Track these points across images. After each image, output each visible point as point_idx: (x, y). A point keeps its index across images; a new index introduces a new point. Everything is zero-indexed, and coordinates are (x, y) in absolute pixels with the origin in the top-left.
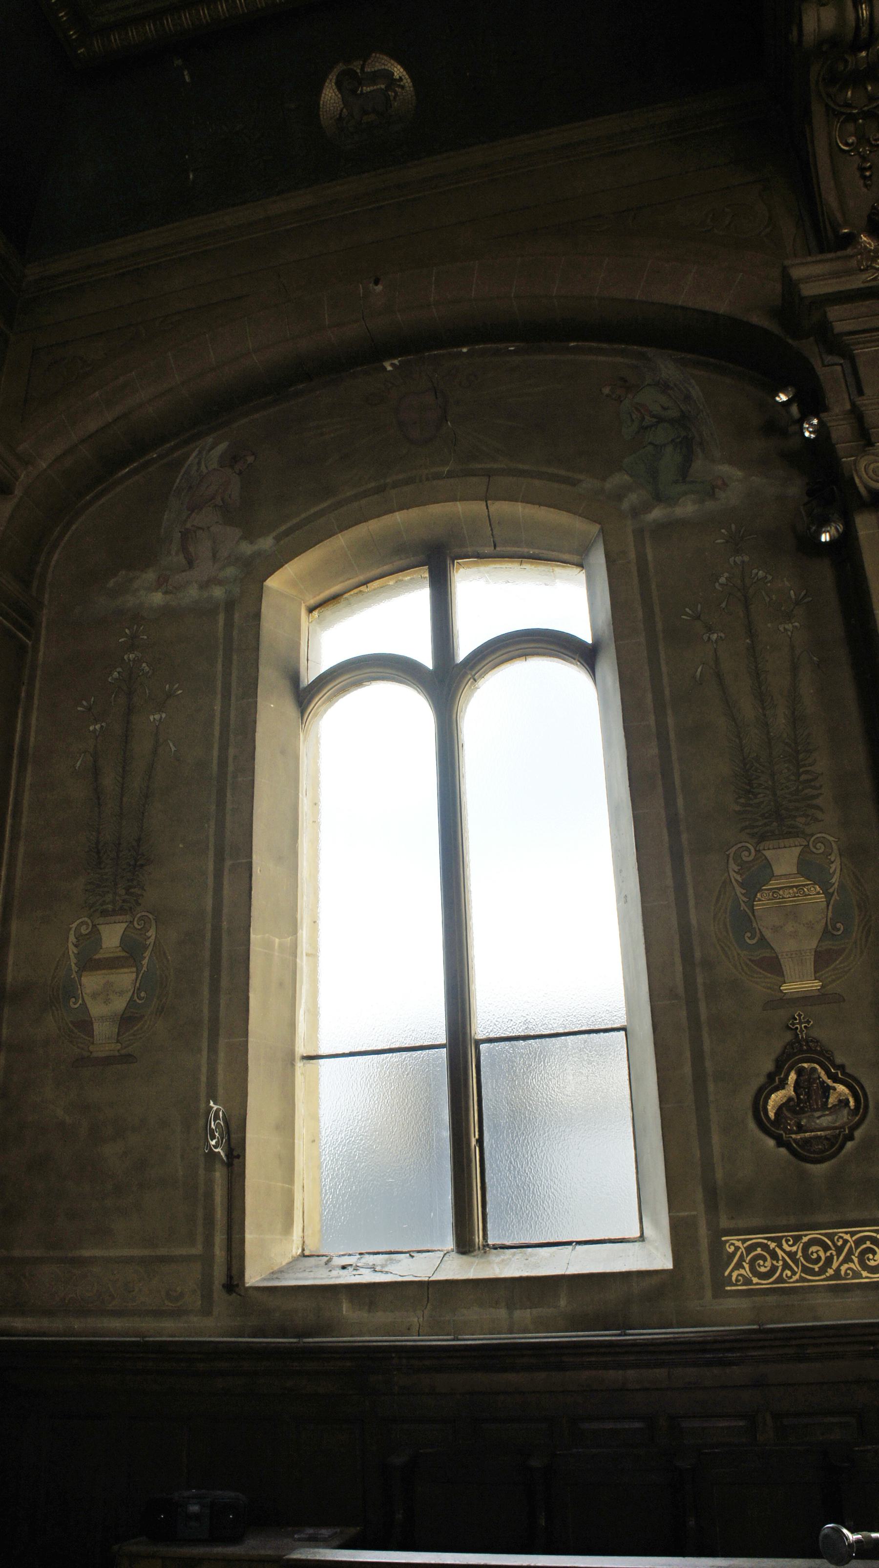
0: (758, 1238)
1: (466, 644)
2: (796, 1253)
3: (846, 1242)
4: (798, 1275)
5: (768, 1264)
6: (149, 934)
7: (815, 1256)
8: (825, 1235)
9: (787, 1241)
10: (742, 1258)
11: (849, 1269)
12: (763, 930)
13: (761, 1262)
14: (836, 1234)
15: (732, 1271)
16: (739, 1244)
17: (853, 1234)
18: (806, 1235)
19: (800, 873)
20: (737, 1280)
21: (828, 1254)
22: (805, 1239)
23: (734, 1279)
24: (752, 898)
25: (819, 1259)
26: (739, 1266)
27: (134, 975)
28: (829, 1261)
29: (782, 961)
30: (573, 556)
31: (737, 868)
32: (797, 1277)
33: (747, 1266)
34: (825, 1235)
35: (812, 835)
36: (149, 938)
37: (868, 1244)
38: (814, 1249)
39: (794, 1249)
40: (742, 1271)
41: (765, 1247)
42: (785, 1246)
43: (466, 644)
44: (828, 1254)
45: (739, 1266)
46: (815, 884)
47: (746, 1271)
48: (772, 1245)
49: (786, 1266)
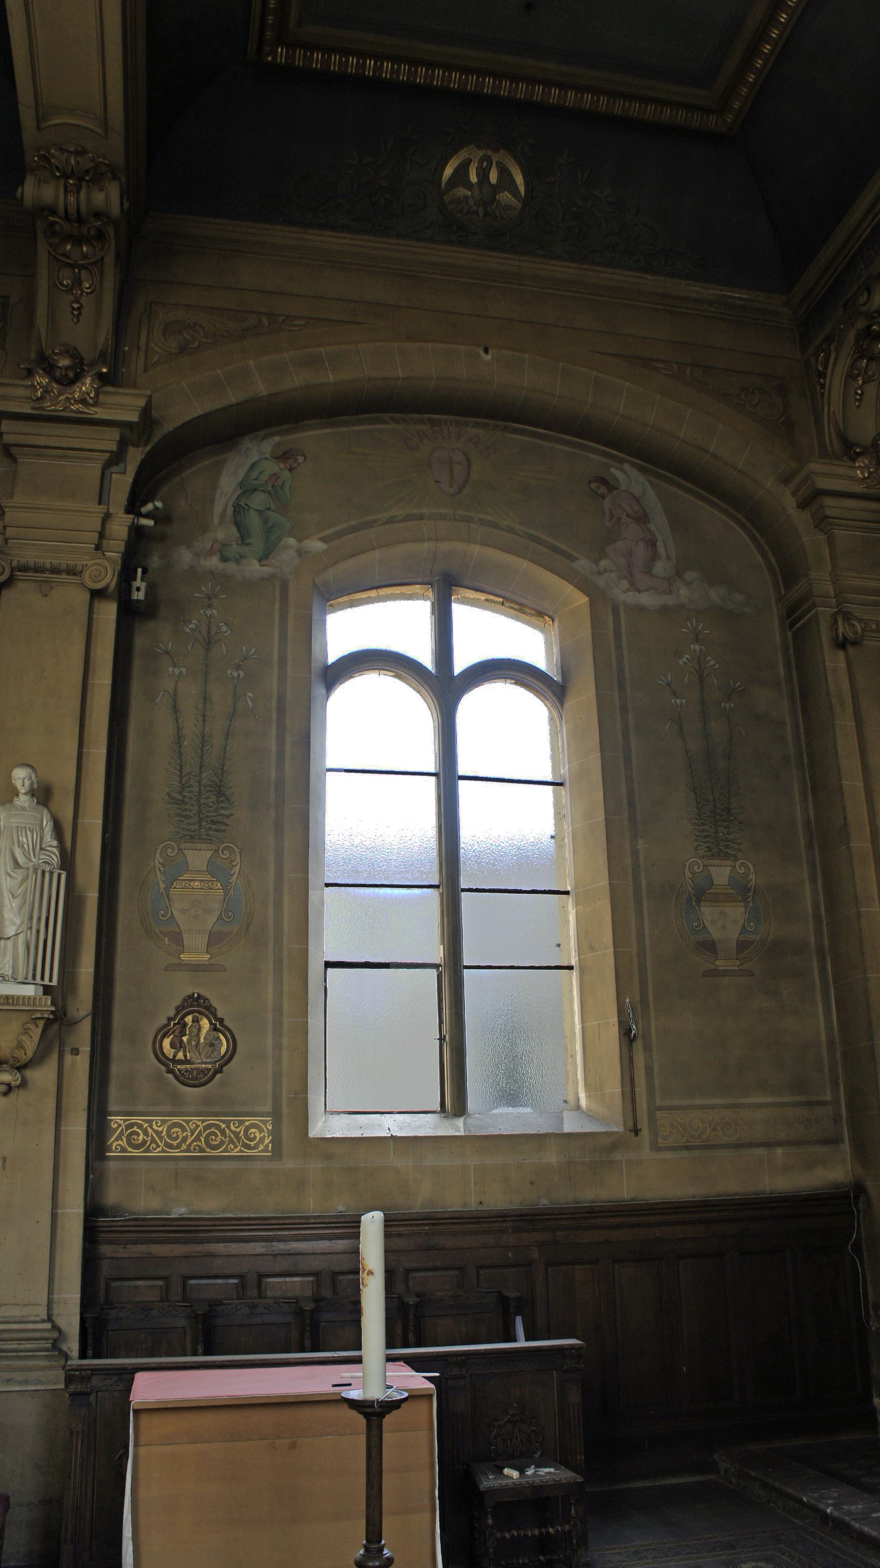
0: (212, 1120)
1: (461, 662)
2: (162, 1132)
3: (198, 1126)
4: (159, 1149)
5: (141, 1138)
6: (750, 877)
7: (175, 1135)
8: (261, 1121)
9: (234, 1124)
10: (122, 1133)
11: (119, 1145)
12: (705, 922)
13: (214, 1138)
14: (191, 1120)
15: (113, 1142)
16: (199, 1123)
17: (203, 1121)
18: (248, 1121)
19: (209, 872)
20: (116, 1149)
21: (185, 1134)
22: (247, 1123)
23: (192, 1148)
24: (169, 886)
25: (255, 1137)
26: (119, 1138)
27: (743, 909)
28: (185, 1139)
29: (184, 936)
30: (424, 598)
31: (162, 861)
32: (159, 1149)
33: (124, 1139)
34: (261, 1121)
35: (223, 843)
36: (235, 866)
37: (213, 1129)
38: (253, 1130)
39: (160, 1129)
40: (120, 1142)
41: (218, 1127)
42: (155, 1127)
43: (461, 662)
44: (185, 1134)
45: (119, 1138)
46: (217, 881)
47: (123, 1143)
48: (223, 1126)
49: (153, 1141)
